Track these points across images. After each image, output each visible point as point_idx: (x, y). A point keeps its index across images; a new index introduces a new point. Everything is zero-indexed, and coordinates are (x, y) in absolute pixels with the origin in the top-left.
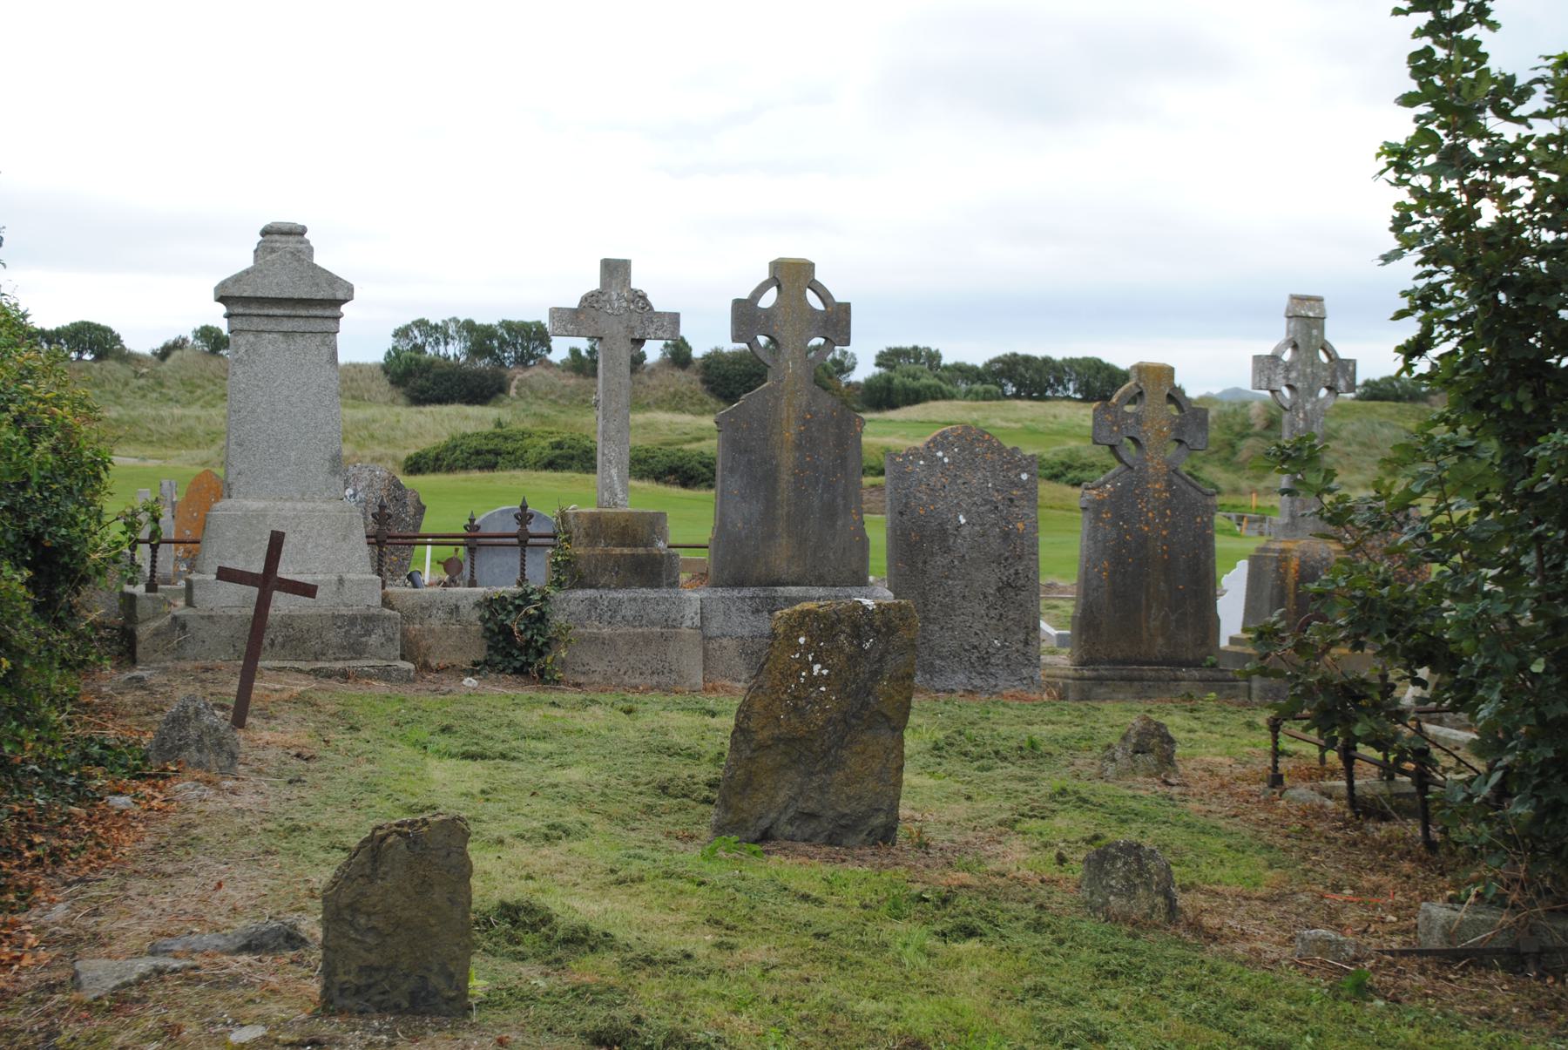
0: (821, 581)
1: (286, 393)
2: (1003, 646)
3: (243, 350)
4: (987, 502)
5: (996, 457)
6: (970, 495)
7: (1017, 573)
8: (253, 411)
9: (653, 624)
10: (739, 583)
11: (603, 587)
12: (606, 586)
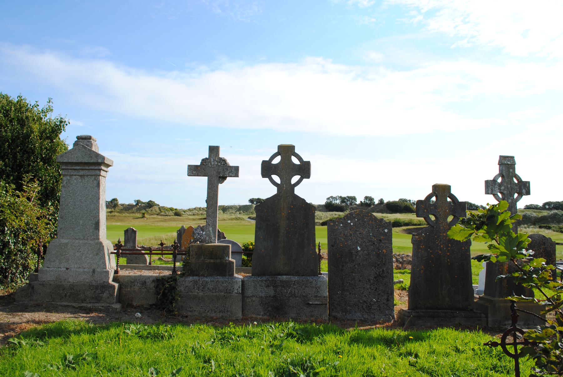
0: (297, 274)
1: (80, 198)
2: (377, 301)
3: (65, 182)
4: (370, 241)
5: (374, 223)
6: (362, 239)
7: (383, 271)
8: (68, 205)
9: (221, 291)
10: (262, 274)
11: (202, 275)
12: (203, 275)
